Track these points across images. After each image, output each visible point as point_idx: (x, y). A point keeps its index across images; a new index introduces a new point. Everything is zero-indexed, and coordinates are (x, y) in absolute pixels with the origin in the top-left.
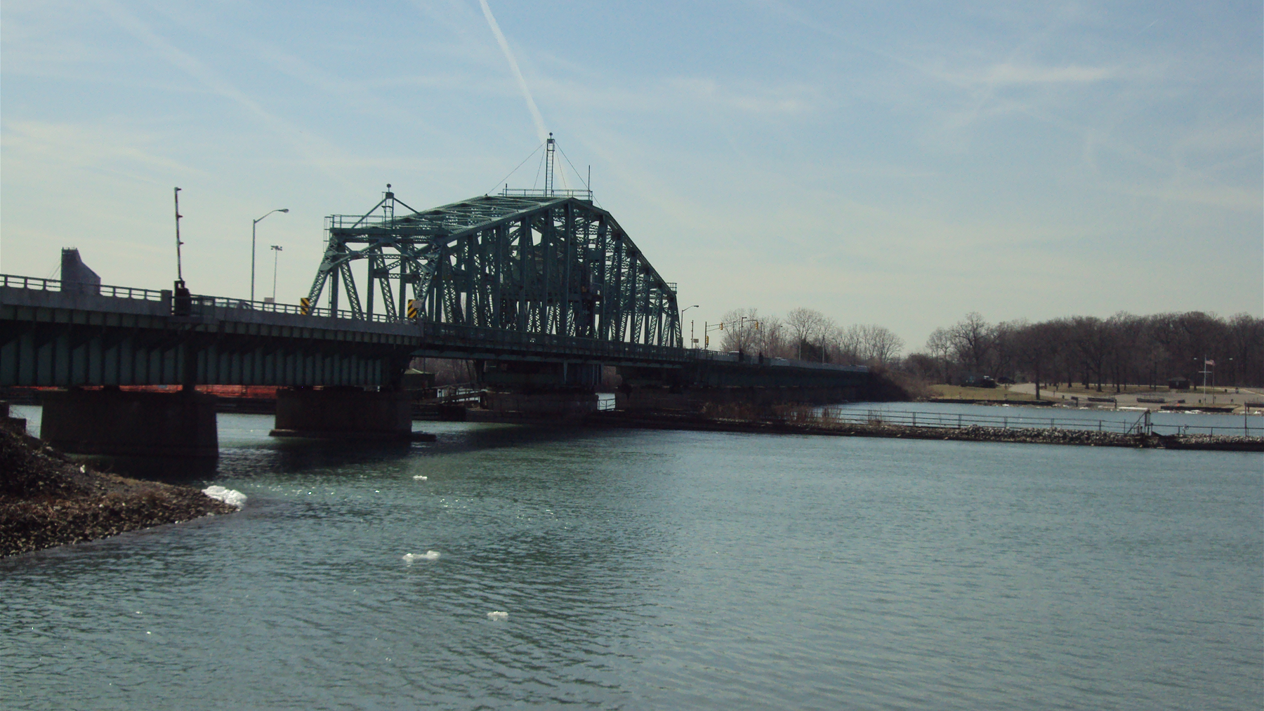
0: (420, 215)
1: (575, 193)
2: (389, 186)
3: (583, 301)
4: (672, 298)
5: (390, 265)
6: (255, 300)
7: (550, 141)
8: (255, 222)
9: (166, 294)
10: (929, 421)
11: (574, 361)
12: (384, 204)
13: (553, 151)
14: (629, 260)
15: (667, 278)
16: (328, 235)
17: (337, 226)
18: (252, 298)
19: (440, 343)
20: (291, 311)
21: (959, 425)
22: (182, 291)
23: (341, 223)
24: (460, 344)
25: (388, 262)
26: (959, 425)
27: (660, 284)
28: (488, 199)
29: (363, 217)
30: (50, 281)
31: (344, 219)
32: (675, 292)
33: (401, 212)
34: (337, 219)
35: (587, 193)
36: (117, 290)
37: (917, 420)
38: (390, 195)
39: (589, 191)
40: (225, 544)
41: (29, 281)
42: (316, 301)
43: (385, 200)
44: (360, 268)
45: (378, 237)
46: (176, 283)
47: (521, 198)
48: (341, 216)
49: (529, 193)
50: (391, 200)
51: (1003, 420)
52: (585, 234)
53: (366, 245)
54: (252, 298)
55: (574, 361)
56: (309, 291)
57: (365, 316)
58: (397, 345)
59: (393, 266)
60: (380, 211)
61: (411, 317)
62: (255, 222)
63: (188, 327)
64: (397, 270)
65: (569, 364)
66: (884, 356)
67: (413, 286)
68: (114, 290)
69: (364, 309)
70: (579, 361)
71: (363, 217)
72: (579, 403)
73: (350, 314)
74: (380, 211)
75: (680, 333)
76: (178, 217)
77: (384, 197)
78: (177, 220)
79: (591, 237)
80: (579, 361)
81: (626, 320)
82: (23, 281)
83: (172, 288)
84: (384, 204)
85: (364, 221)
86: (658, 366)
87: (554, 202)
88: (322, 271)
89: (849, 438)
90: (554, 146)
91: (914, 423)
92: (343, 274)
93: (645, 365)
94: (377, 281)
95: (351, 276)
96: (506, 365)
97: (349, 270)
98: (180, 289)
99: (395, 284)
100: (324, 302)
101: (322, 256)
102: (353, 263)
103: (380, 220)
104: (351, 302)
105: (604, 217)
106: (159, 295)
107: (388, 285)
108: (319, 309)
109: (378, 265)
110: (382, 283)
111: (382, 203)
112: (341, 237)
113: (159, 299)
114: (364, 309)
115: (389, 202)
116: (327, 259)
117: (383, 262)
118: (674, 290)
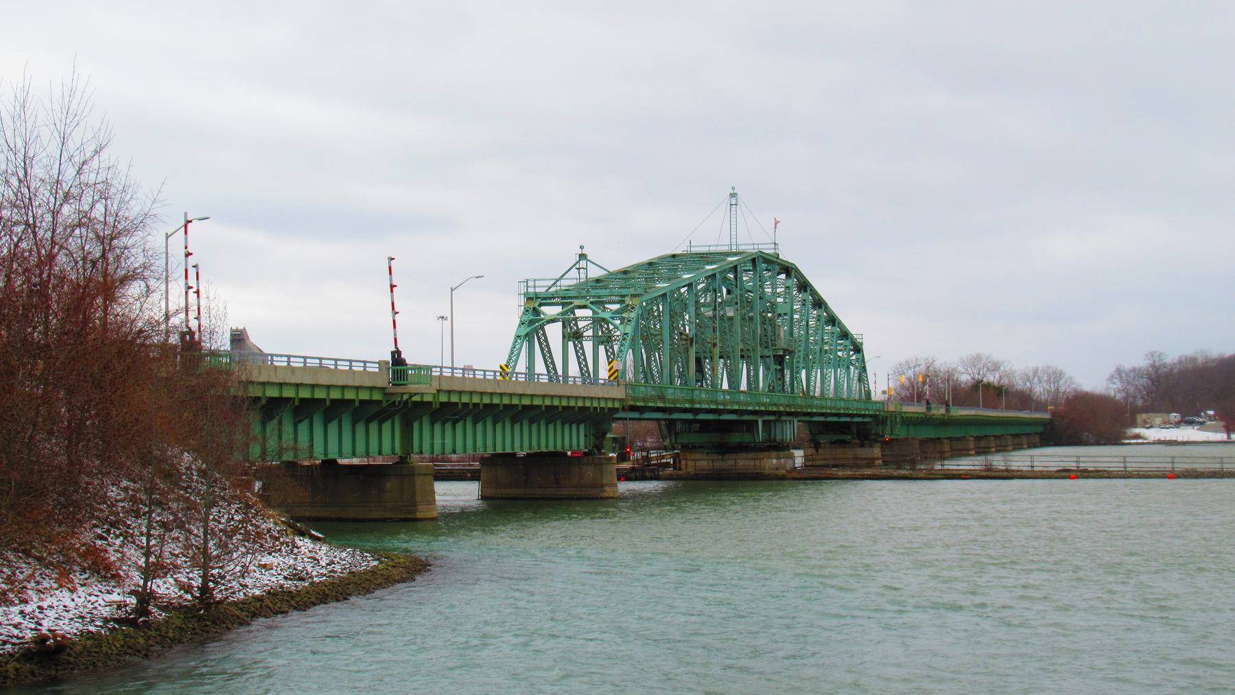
0: (611, 273)
1: (760, 247)
2: (582, 247)
3: (774, 356)
4: (858, 349)
5: (584, 327)
6: (455, 366)
7: (733, 195)
8: (452, 290)
9: (382, 364)
10: (1141, 465)
11: (767, 418)
12: (577, 266)
13: (736, 205)
14: (815, 312)
15: (853, 329)
16: (522, 300)
17: (531, 290)
18: (453, 364)
19: (642, 404)
20: (490, 376)
21: (1125, 468)
22: (397, 358)
23: (535, 287)
24: (660, 405)
25: (581, 324)
26: (1125, 468)
27: (845, 335)
28: (674, 256)
29: (557, 280)
30: (277, 356)
31: (538, 283)
32: (862, 344)
33: (595, 273)
34: (530, 283)
35: (773, 246)
36: (339, 363)
37: (1128, 465)
38: (583, 256)
39: (775, 244)
40: (1045, 532)
41: (292, 359)
42: (514, 367)
43: (578, 262)
44: (554, 332)
45: (566, 299)
46: (393, 353)
47: (707, 254)
48: (535, 280)
49: (713, 249)
50: (585, 261)
51: (1170, 460)
52: (772, 288)
53: (559, 309)
54: (453, 364)
55: (767, 418)
56: (507, 357)
57: (561, 378)
58: (579, 407)
59: (586, 328)
60: (574, 272)
61: (612, 379)
62: (452, 290)
63: (406, 397)
64: (590, 333)
65: (764, 422)
66: (109, 278)
67: (606, 348)
68: (289, 359)
69: (560, 372)
70: (772, 418)
71: (557, 280)
72: (774, 461)
73: (547, 377)
74: (574, 272)
75: (868, 385)
76: (392, 287)
77: (578, 259)
78: (392, 291)
79: (778, 290)
80: (772, 418)
81: (816, 373)
82: (302, 360)
83: (389, 358)
84: (577, 266)
85: (558, 284)
86: (847, 419)
87: (745, 255)
88: (518, 337)
89: (767, 500)
90: (737, 199)
91: (1032, 467)
92: (539, 339)
93: (835, 419)
94: (602, 348)
95: (546, 340)
96: (698, 425)
97: (544, 334)
98: (187, 342)
99: (588, 346)
100: (521, 367)
101: (518, 321)
102: (548, 328)
103: (574, 282)
104: (547, 367)
105: (788, 270)
106: (377, 365)
107: (582, 348)
108: (517, 373)
109: (571, 328)
110: (575, 346)
111: (575, 265)
112: (534, 302)
113: (377, 370)
114: (560, 372)
115: (583, 263)
116: (523, 324)
117: (576, 325)
118: (860, 341)
